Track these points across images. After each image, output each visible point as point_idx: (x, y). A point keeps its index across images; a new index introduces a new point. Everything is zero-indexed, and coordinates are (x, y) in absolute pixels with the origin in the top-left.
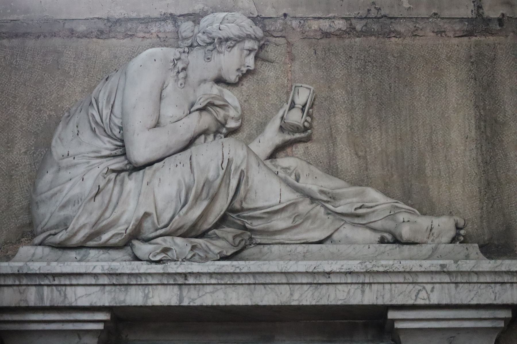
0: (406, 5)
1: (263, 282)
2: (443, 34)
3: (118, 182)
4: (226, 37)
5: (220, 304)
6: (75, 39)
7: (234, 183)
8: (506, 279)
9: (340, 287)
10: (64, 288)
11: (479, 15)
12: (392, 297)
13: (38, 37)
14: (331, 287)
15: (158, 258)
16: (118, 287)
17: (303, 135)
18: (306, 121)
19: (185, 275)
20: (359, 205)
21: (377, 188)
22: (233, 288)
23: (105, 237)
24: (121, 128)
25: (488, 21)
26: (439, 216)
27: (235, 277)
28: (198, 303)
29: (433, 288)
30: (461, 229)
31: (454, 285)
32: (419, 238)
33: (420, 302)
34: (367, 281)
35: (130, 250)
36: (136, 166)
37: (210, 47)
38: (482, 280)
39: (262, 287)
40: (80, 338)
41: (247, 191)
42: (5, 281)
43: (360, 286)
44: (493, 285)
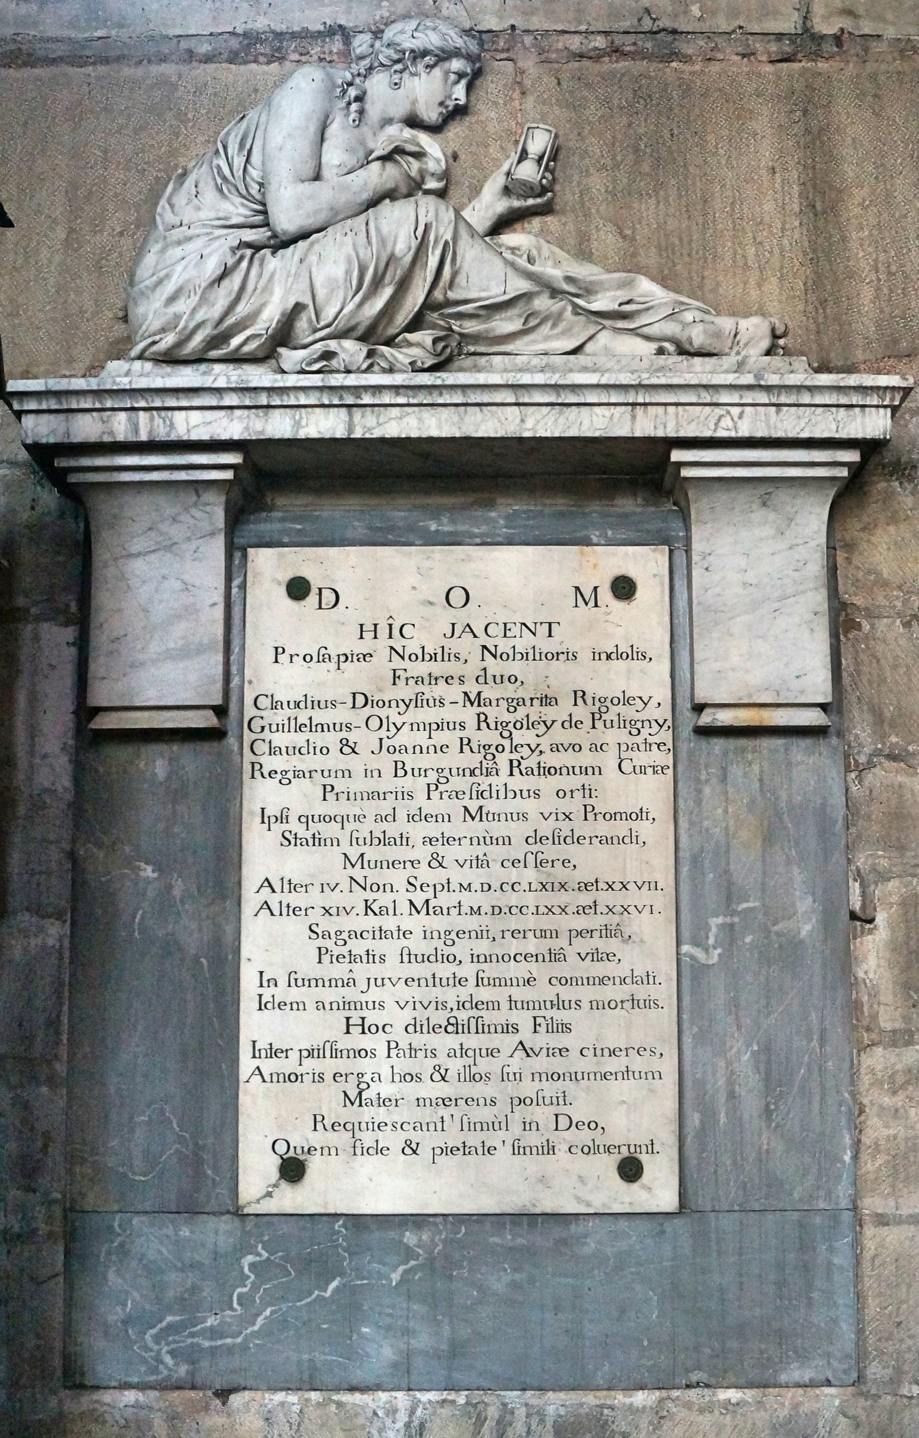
0: (695, 10)
1: (478, 401)
2: (752, 58)
3: (256, 262)
4: (422, 49)
5: (413, 436)
6: (195, 64)
7: (433, 261)
8: (855, 399)
9: (597, 409)
10: (170, 413)
11: (806, 30)
12: (678, 425)
13: (140, 62)
14: (584, 409)
15: (316, 367)
16: (254, 411)
17: (539, 200)
18: (543, 177)
19: (356, 390)
20: (626, 299)
21: (653, 279)
22: (433, 412)
23: (235, 342)
24: (261, 185)
25: (819, 39)
26: (746, 316)
27: (436, 393)
28: (377, 434)
29: (742, 413)
30: (780, 337)
31: (773, 409)
32: (716, 346)
33: (721, 433)
34: (640, 400)
35: (276, 364)
36: (284, 238)
37: (399, 67)
38: (818, 400)
39: (477, 409)
40: (199, 496)
41: (455, 275)
42: (78, 402)
43: (630, 408)
44: (834, 409)
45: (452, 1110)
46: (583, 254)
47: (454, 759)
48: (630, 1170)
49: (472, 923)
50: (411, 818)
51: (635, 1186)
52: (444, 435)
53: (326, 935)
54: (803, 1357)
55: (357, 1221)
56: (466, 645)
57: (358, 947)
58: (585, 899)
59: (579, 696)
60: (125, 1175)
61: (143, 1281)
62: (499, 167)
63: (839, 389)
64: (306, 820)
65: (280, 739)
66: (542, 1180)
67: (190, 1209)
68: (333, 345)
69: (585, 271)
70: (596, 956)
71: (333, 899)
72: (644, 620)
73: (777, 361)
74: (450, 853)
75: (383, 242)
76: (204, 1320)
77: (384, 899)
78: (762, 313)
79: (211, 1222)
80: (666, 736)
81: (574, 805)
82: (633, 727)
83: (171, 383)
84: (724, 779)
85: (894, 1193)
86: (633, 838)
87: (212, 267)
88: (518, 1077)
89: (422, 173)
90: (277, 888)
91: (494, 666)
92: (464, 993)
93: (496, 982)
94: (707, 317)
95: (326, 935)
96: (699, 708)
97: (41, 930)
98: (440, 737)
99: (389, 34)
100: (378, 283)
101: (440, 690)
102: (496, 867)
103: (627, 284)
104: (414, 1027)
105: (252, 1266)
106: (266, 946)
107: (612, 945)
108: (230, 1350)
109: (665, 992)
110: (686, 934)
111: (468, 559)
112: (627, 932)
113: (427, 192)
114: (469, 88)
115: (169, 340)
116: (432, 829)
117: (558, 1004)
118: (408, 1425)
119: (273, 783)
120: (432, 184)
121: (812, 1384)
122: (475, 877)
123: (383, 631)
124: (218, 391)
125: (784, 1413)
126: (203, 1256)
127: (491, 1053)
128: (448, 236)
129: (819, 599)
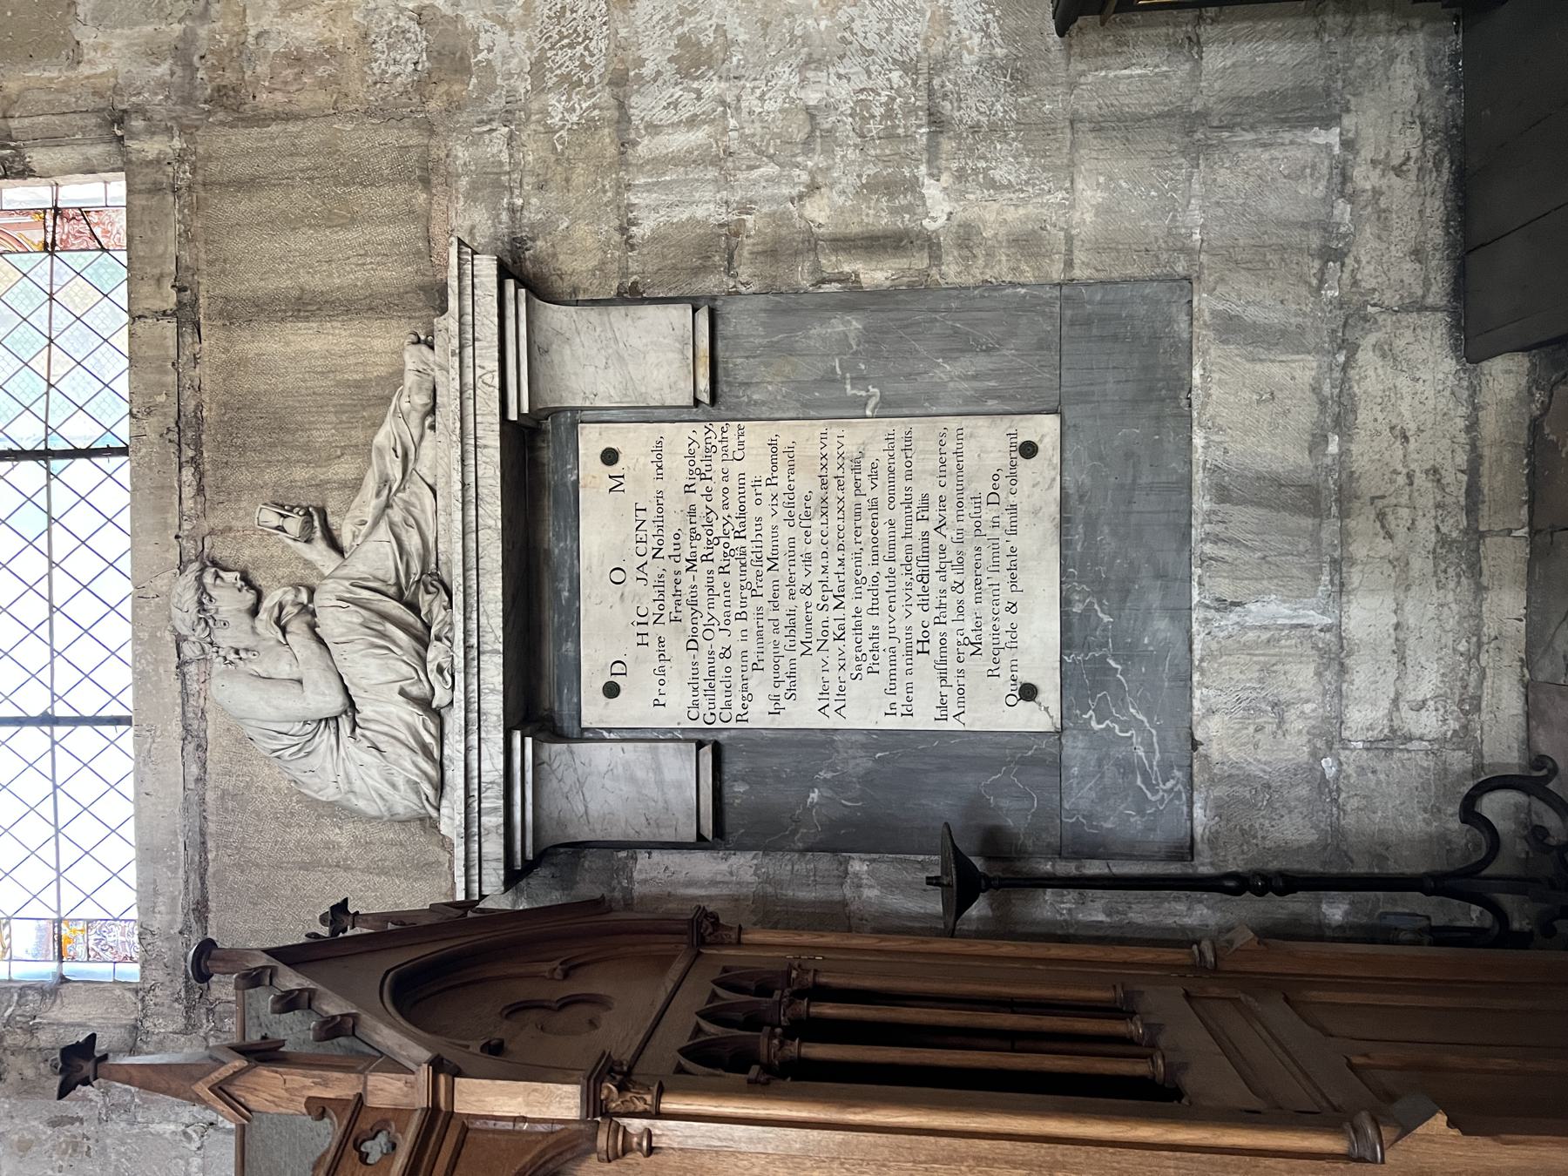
7: (366, 594)
11: (174, 314)
12: (492, 413)
15: (449, 679)
19: (467, 648)
21: (375, 433)
23: (428, 739)
24: (305, 723)
28: (500, 633)
32: (428, 385)
33: (496, 382)
37: (211, 622)
41: (376, 579)
45: (984, 578)
46: (356, 485)
47: (734, 578)
48: (1029, 450)
49: (850, 564)
50: (776, 609)
51: (1040, 446)
52: (500, 584)
53: (859, 668)
54: (1170, 321)
55: (1066, 645)
56: (653, 570)
57: (867, 645)
58: (833, 484)
59: (689, 490)
60: (1033, 815)
61: (1111, 802)
62: (288, 546)
63: (460, 293)
64: (777, 683)
65: (720, 702)
66: (1035, 513)
67: (1057, 765)
68: (431, 667)
69: (371, 483)
70: (874, 476)
71: (834, 663)
72: (633, 441)
73: (438, 342)
74: (801, 580)
75: (351, 631)
76: (1140, 757)
77: (833, 627)
78: (399, 353)
79: (1067, 751)
80: (717, 426)
81: (766, 492)
82: (710, 450)
83: (461, 782)
84: (748, 384)
85: (1049, 254)
86: (790, 450)
87: (370, 758)
88: (960, 531)
89: (295, 604)
90: (825, 703)
91: (668, 549)
92: (900, 570)
93: (892, 546)
94: (406, 393)
95: (859, 668)
96: (697, 402)
97: (856, 875)
98: (719, 589)
99: (184, 631)
100: (383, 635)
101: (685, 588)
102: (810, 548)
103: (380, 451)
104: (924, 606)
105: (1099, 722)
106: (866, 710)
107: (866, 465)
108: (1162, 740)
109: (899, 427)
110: (859, 412)
111: (589, 568)
112: (856, 455)
113: (311, 600)
114: (226, 570)
115: (427, 788)
116: (784, 593)
117: (908, 503)
118: (1218, 610)
119: (752, 707)
120: (304, 597)
121: (1190, 314)
122: (816, 567)
123: (643, 629)
124: (467, 749)
125: (1211, 335)
126: (1093, 759)
127: (943, 551)
128: (347, 583)
129: (616, 313)
